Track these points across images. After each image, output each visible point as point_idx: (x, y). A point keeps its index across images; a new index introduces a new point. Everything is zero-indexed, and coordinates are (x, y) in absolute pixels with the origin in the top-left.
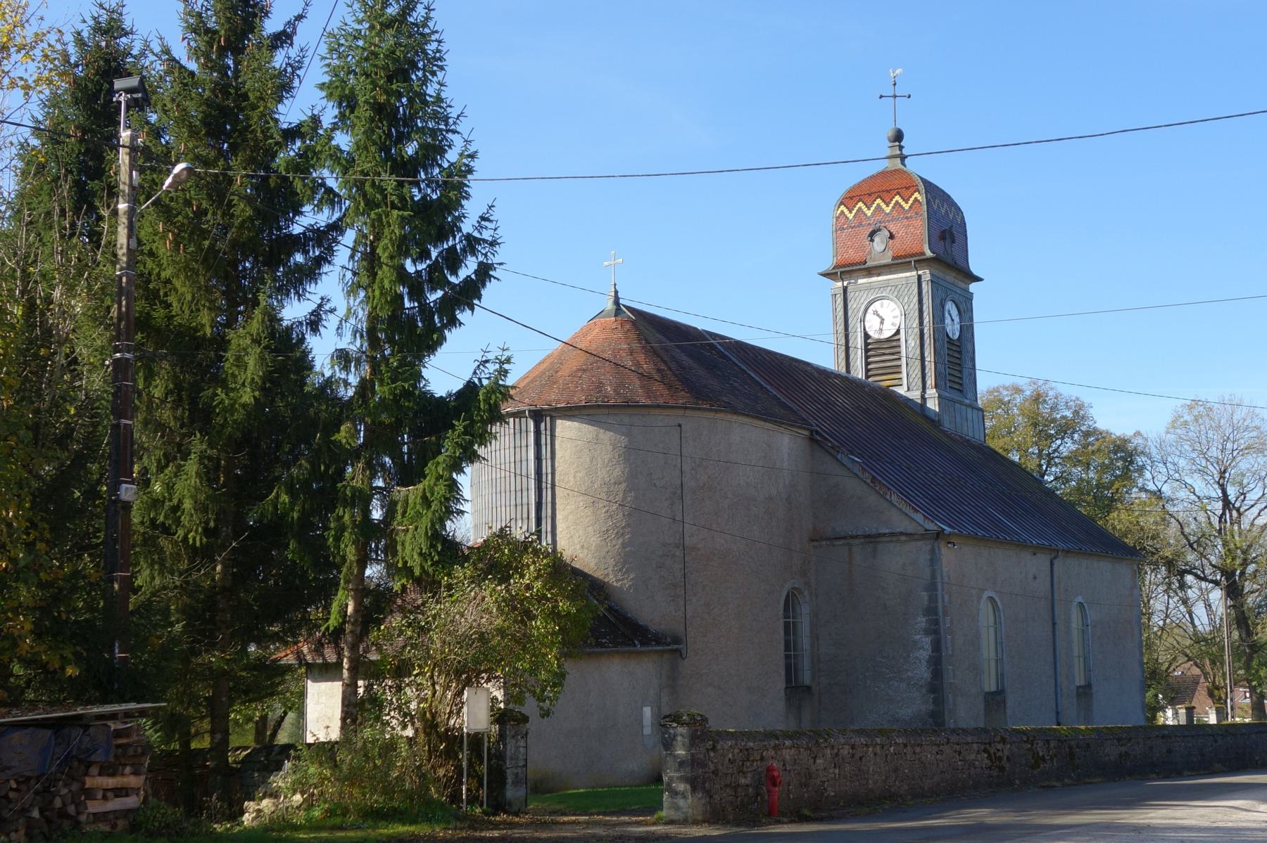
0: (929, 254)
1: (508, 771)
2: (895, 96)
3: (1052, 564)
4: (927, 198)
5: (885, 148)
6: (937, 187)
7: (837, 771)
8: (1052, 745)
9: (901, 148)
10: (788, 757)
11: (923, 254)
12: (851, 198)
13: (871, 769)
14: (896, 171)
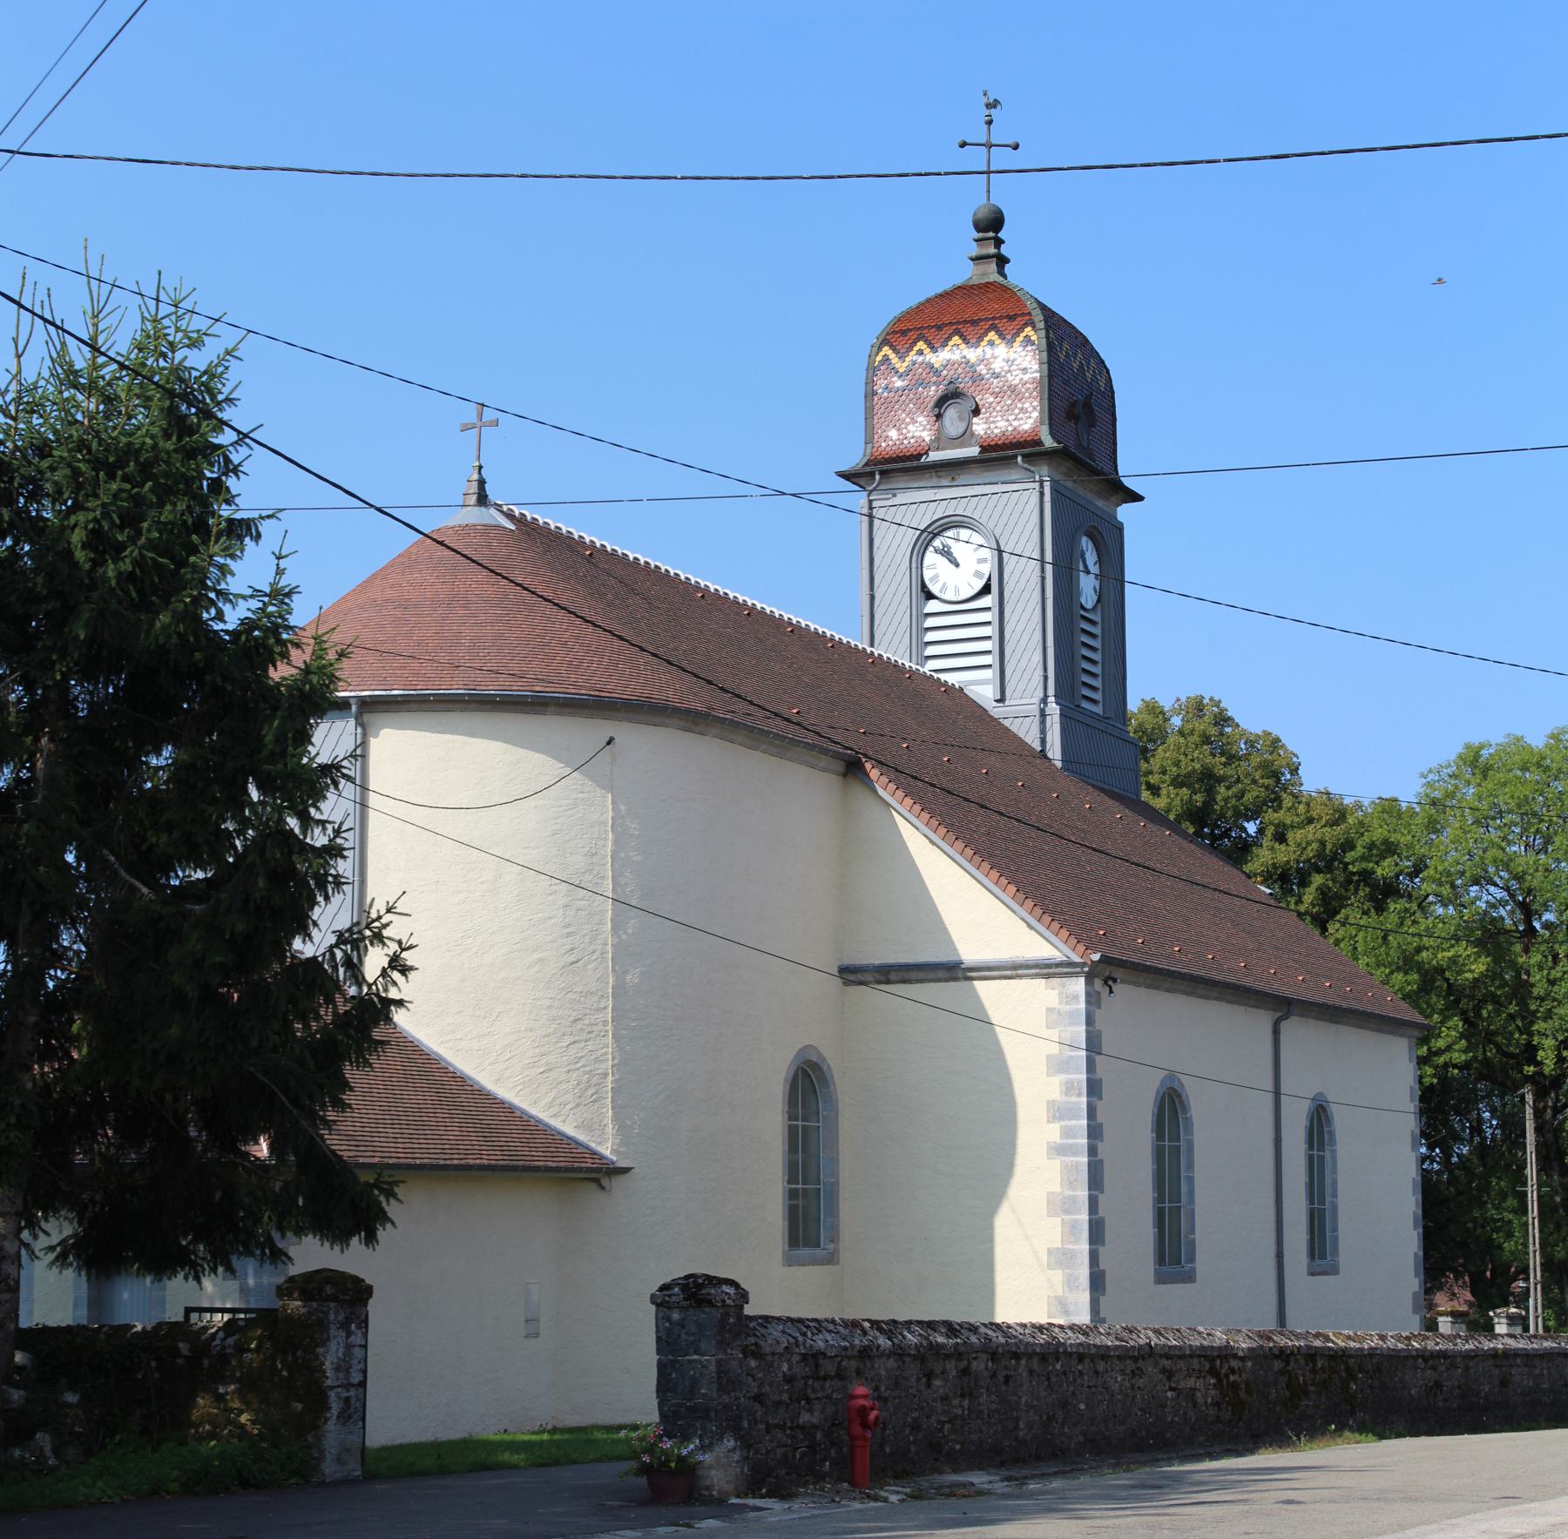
0: (1049, 442)
1: (332, 1394)
2: (989, 146)
3: (1276, 1033)
4: (1048, 337)
5: (967, 242)
6: (1065, 321)
7: (966, 1403)
8: (1319, 1365)
9: (999, 242)
10: (883, 1372)
11: (1039, 443)
12: (904, 333)
13: (1023, 1400)
14: (987, 285)
